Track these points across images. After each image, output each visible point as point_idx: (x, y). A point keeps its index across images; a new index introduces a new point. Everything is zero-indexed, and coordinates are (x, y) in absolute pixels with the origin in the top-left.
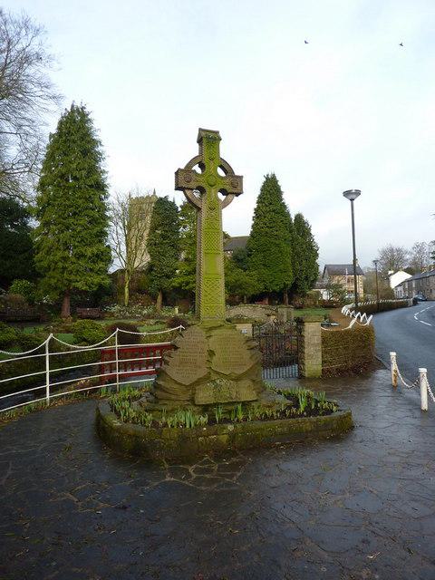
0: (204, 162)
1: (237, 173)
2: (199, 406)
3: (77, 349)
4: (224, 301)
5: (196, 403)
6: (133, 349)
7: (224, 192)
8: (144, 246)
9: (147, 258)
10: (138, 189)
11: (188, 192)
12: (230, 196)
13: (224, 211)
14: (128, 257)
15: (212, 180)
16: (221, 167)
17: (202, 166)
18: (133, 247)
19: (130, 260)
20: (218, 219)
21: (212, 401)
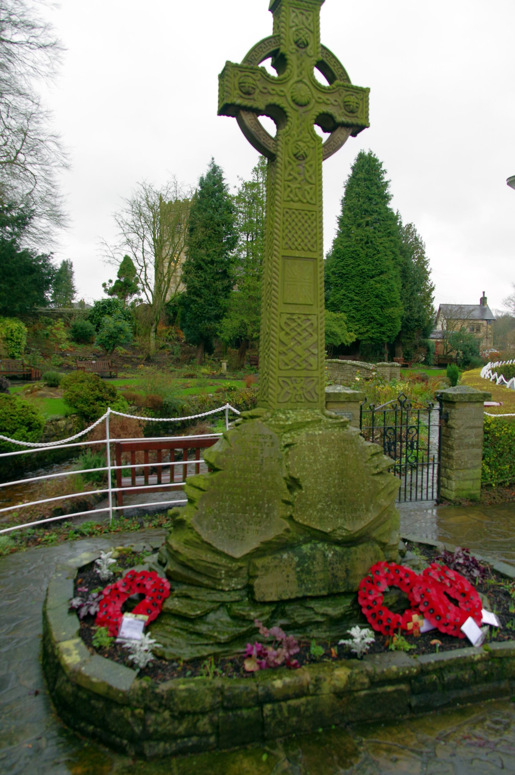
0: (283, 50)
1: (356, 81)
2: (265, 603)
3: (21, 448)
4: (207, 471)
5: (258, 597)
6: (172, 446)
7: (327, 122)
8: (180, 272)
9: (183, 288)
10: (176, 184)
11: (247, 118)
12: (340, 132)
13: (326, 164)
14: (158, 287)
15: (304, 92)
16: (322, 67)
17: (280, 63)
18: (165, 271)
19: (159, 292)
20: (279, 689)
21: (292, 591)
